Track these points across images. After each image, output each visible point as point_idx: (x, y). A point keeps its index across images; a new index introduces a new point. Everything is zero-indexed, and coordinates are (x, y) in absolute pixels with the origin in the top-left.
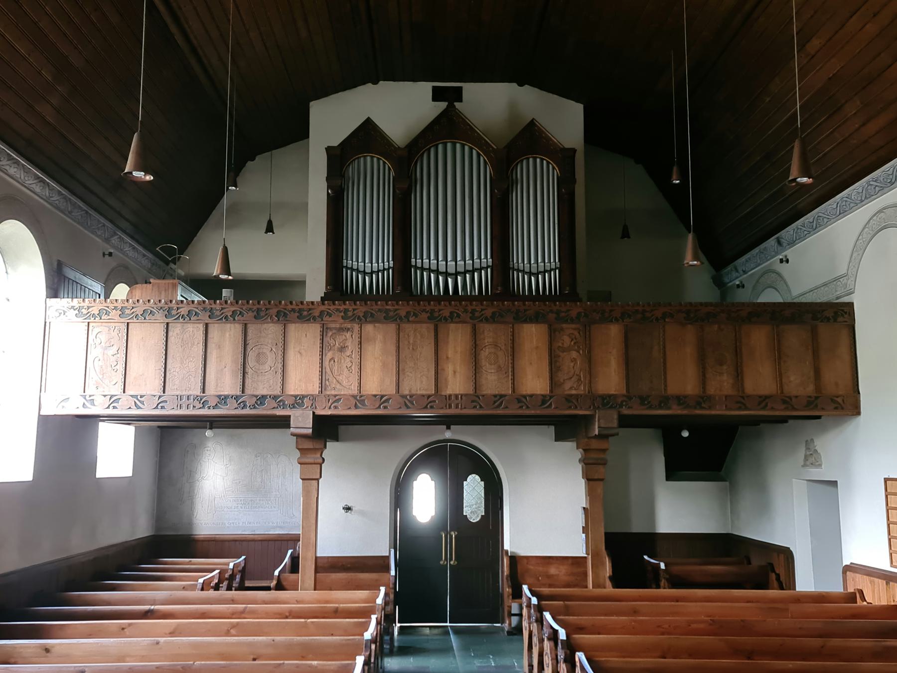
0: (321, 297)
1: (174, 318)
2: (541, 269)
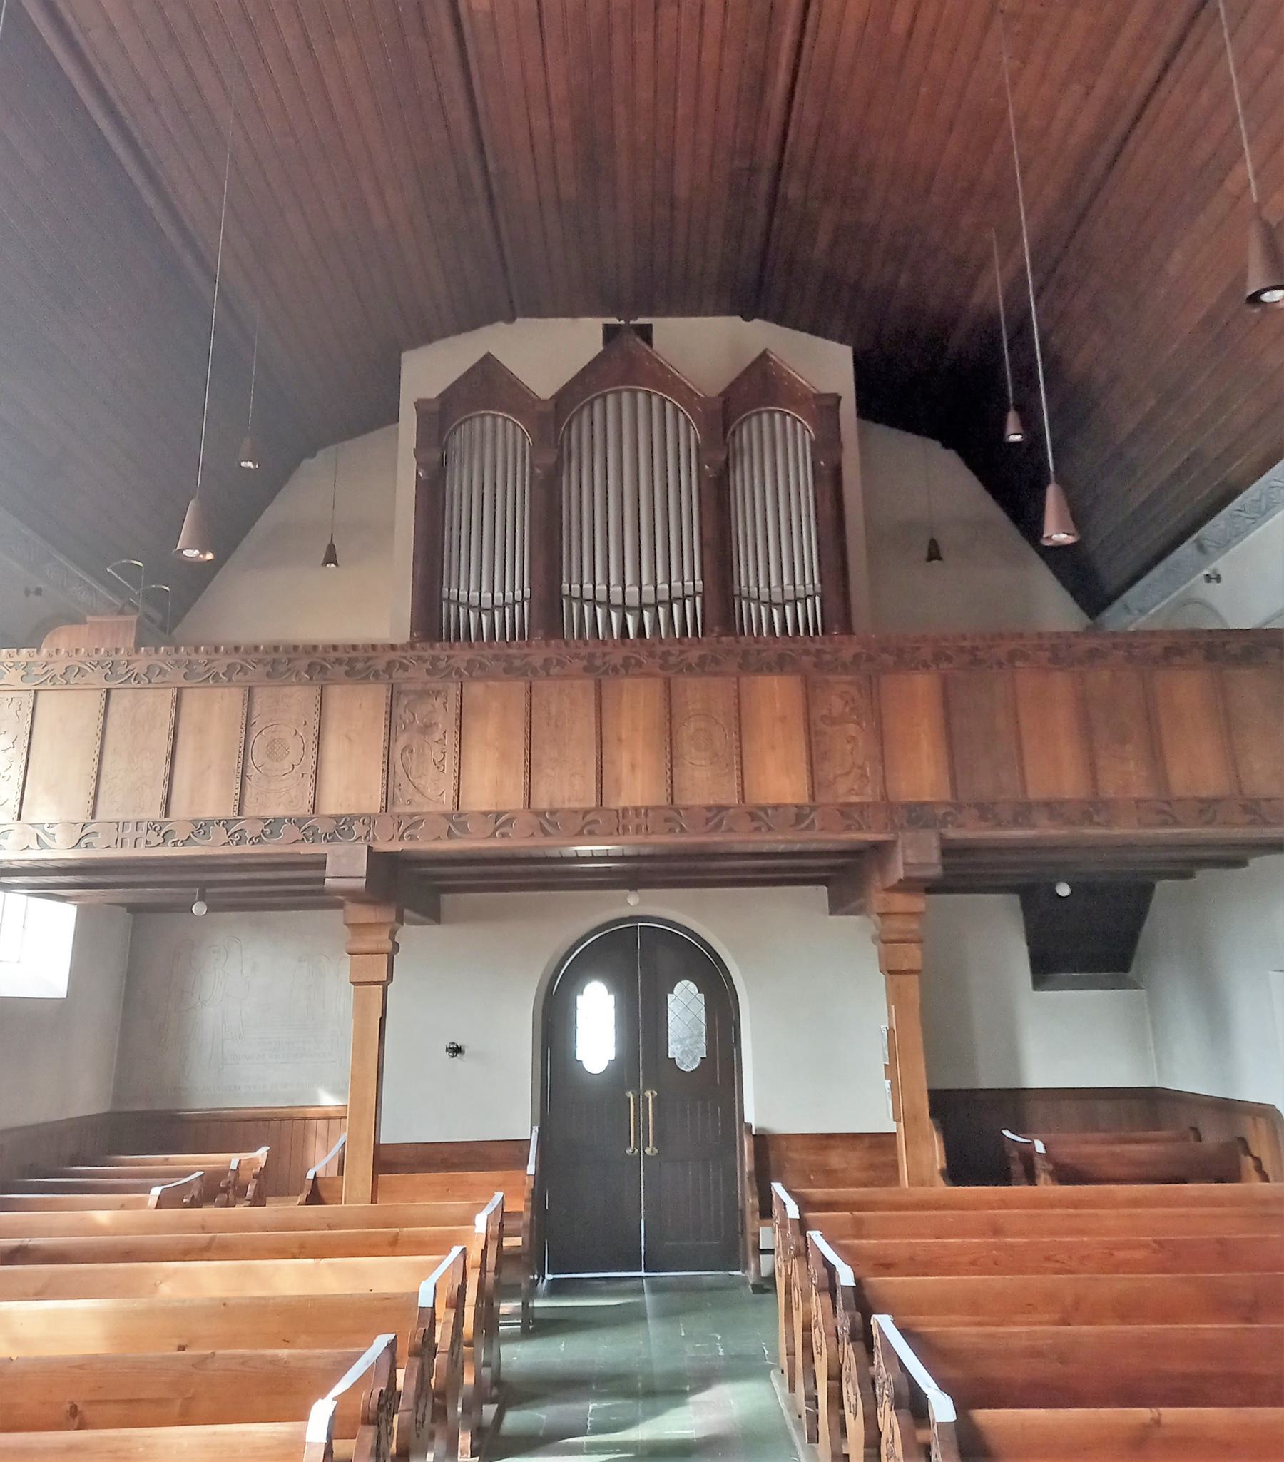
1: (120, 681)
2: (789, 595)
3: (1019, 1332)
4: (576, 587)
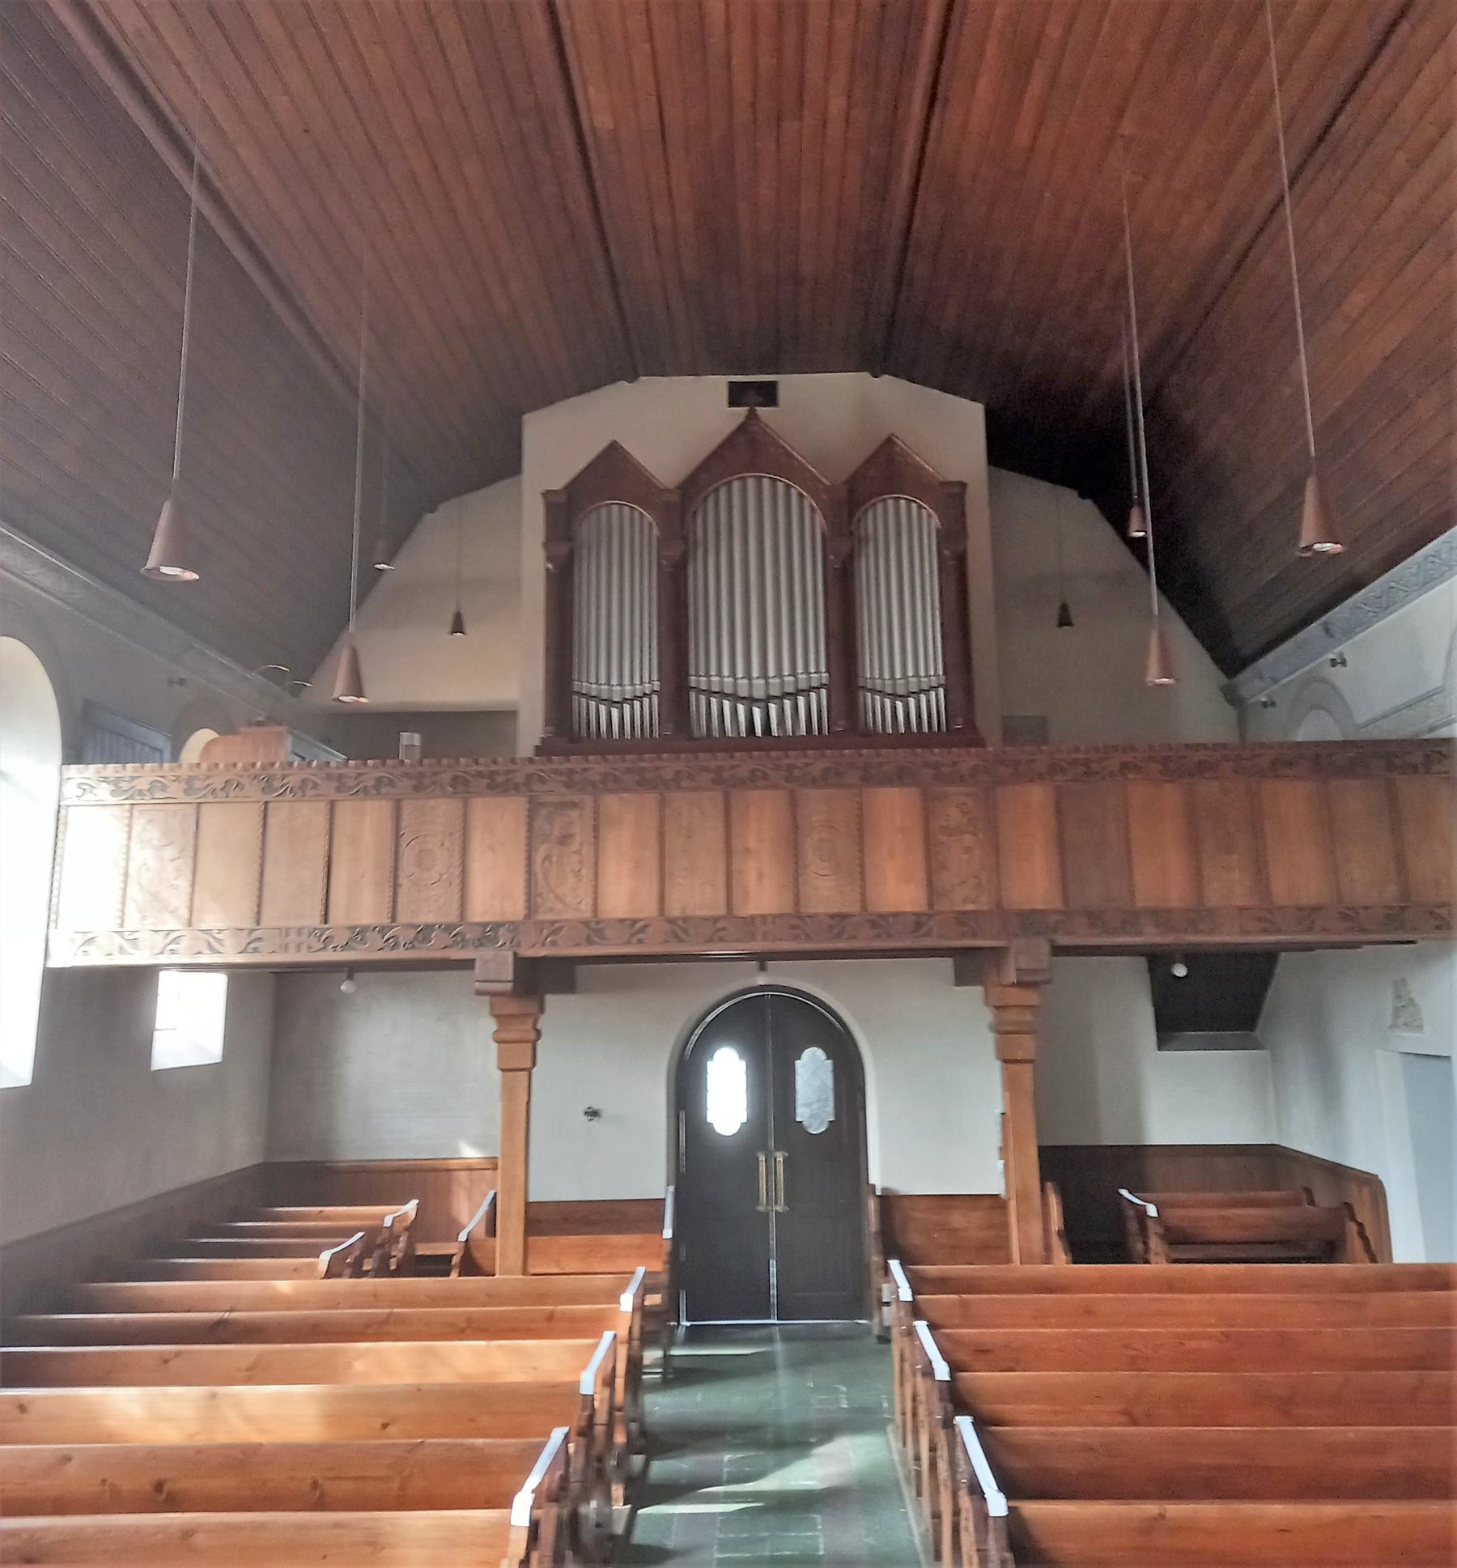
3: (1073, 1432)
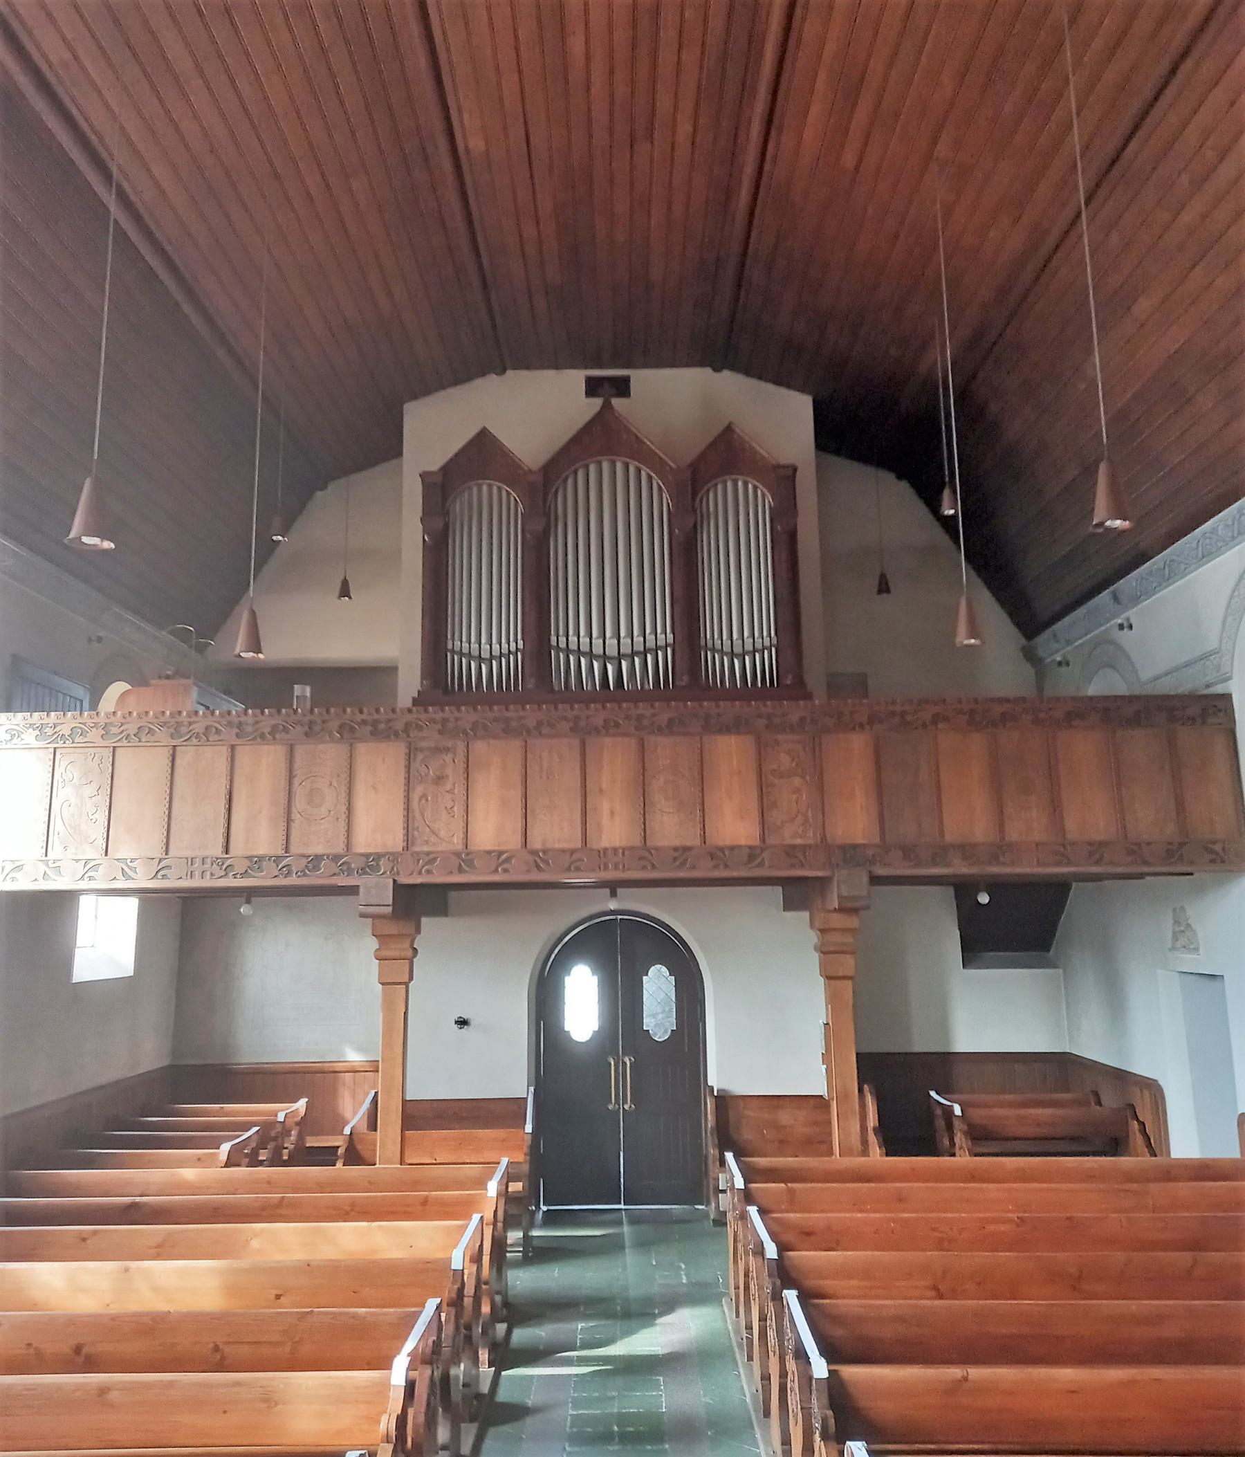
0: (419, 692)
4: (562, 640)
